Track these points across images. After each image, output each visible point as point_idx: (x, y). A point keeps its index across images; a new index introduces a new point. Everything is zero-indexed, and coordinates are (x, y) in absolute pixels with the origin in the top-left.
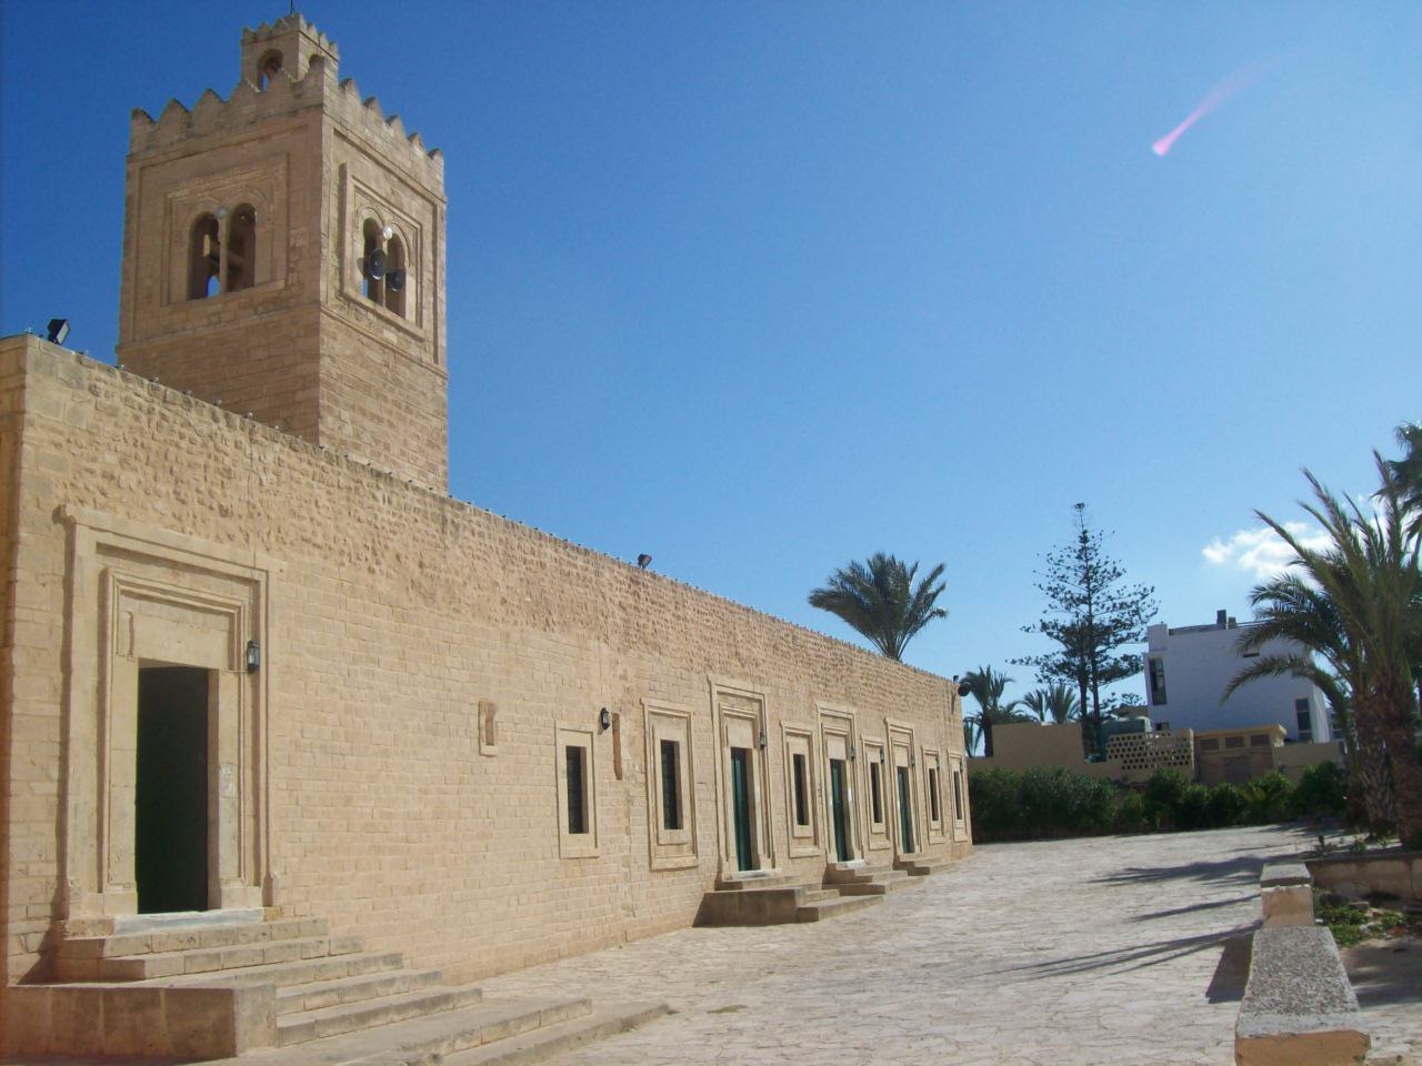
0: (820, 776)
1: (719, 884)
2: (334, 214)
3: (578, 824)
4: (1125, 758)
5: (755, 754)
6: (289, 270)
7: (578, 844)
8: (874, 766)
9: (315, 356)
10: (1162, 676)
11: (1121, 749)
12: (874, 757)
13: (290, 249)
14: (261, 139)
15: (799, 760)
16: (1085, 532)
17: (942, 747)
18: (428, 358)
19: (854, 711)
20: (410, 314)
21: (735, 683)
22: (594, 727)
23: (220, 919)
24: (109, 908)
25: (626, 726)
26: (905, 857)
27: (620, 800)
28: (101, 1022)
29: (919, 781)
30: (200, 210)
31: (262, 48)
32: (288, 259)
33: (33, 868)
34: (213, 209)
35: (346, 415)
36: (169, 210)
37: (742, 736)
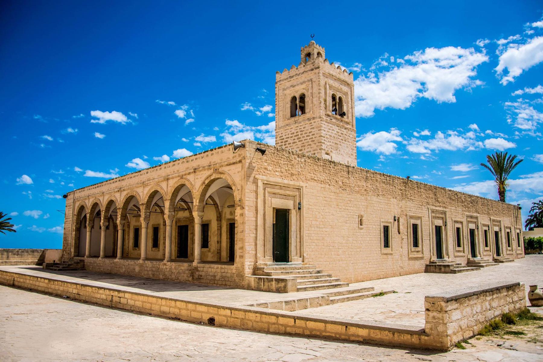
1: (430, 262)
3: (387, 245)
5: (443, 227)
7: (388, 250)
19: (478, 215)
22: (392, 221)
23: (291, 264)
24: (266, 261)
27: (400, 242)
28: (262, 284)
30: (292, 95)
33: (250, 252)
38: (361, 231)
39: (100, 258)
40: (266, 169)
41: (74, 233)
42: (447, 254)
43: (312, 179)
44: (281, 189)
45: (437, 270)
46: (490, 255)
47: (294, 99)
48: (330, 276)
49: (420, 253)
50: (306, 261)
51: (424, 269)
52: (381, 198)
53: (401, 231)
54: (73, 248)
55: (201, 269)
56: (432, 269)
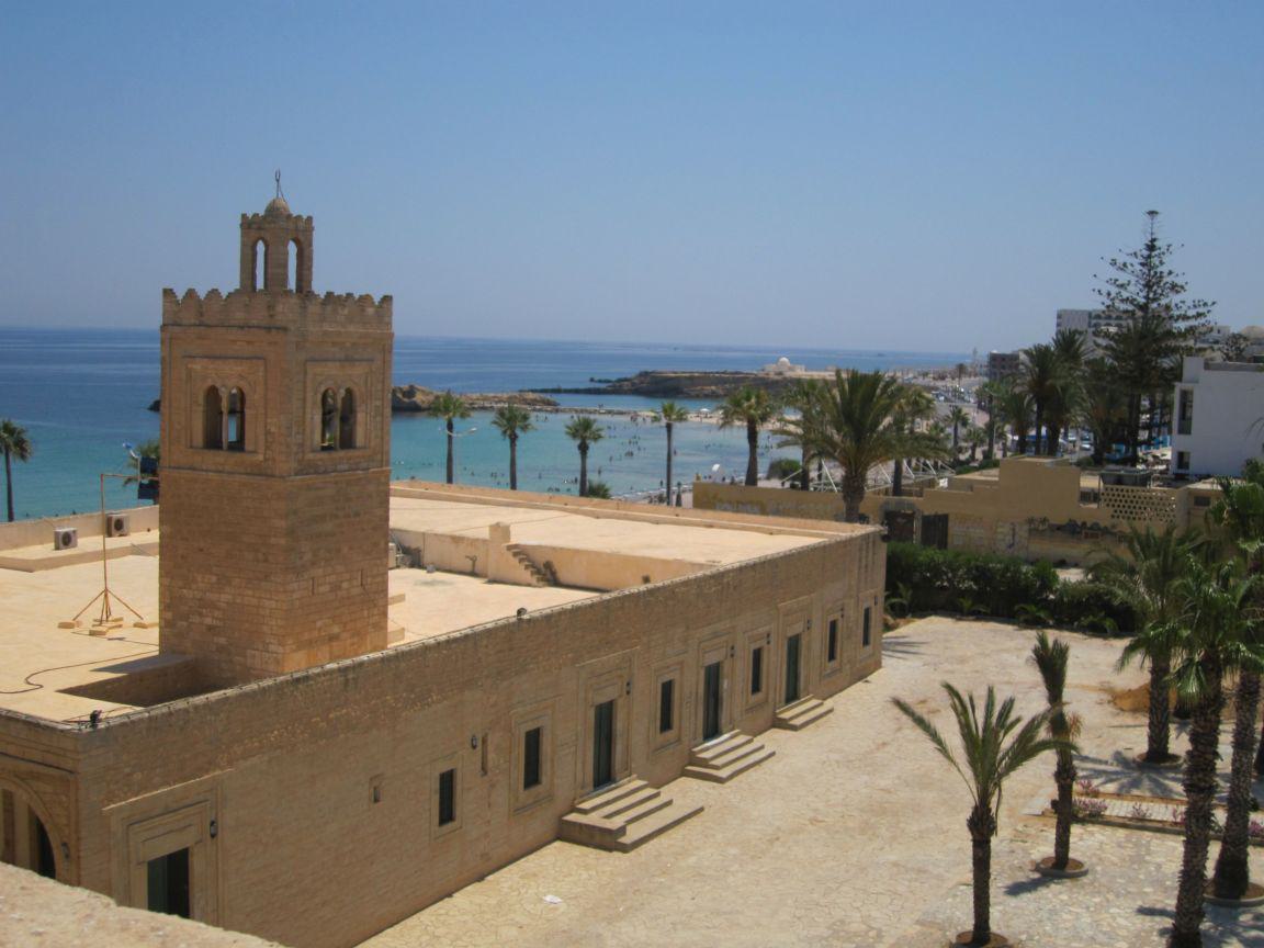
4: (1116, 508)
5: (620, 702)
6: (267, 448)
10: (1191, 406)
11: (1113, 498)
13: (267, 433)
14: (249, 343)
16: (1153, 240)
30: (210, 383)
32: (266, 439)
53: (490, 764)
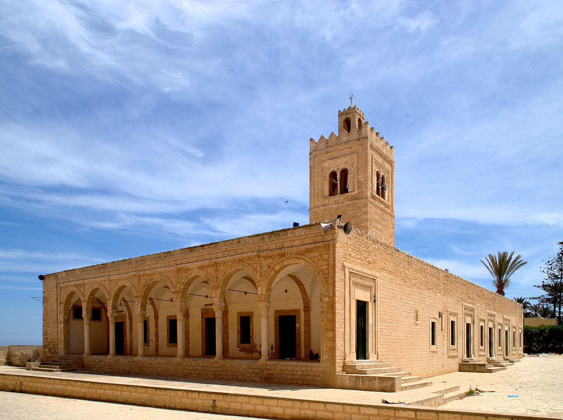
0: (486, 332)
1: (463, 361)
2: (370, 171)
3: (433, 343)
6: (359, 188)
7: (433, 348)
8: (500, 330)
9: (366, 213)
12: (500, 327)
13: (359, 182)
15: (482, 327)
17: (516, 323)
18: (390, 211)
19: (496, 313)
20: (386, 199)
21: (469, 305)
22: (437, 317)
23: (370, 362)
24: (352, 357)
25: (444, 316)
26: (506, 357)
27: (443, 336)
28: (361, 383)
29: (510, 335)
30: (332, 170)
31: (344, 117)
34: (335, 169)
35: (373, 230)
36: (322, 170)
37: (469, 320)
38: (417, 327)
39: (110, 356)
40: (350, 255)
41: (62, 325)
42: (474, 354)
43: (384, 269)
44: (361, 278)
45: (472, 369)
46: (501, 355)
47: (333, 175)
48: (410, 374)
49: (455, 351)
50: (379, 358)
51: (458, 368)
52: (430, 292)
54: (62, 343)
55: (273, 367)
56: (466, 368)
